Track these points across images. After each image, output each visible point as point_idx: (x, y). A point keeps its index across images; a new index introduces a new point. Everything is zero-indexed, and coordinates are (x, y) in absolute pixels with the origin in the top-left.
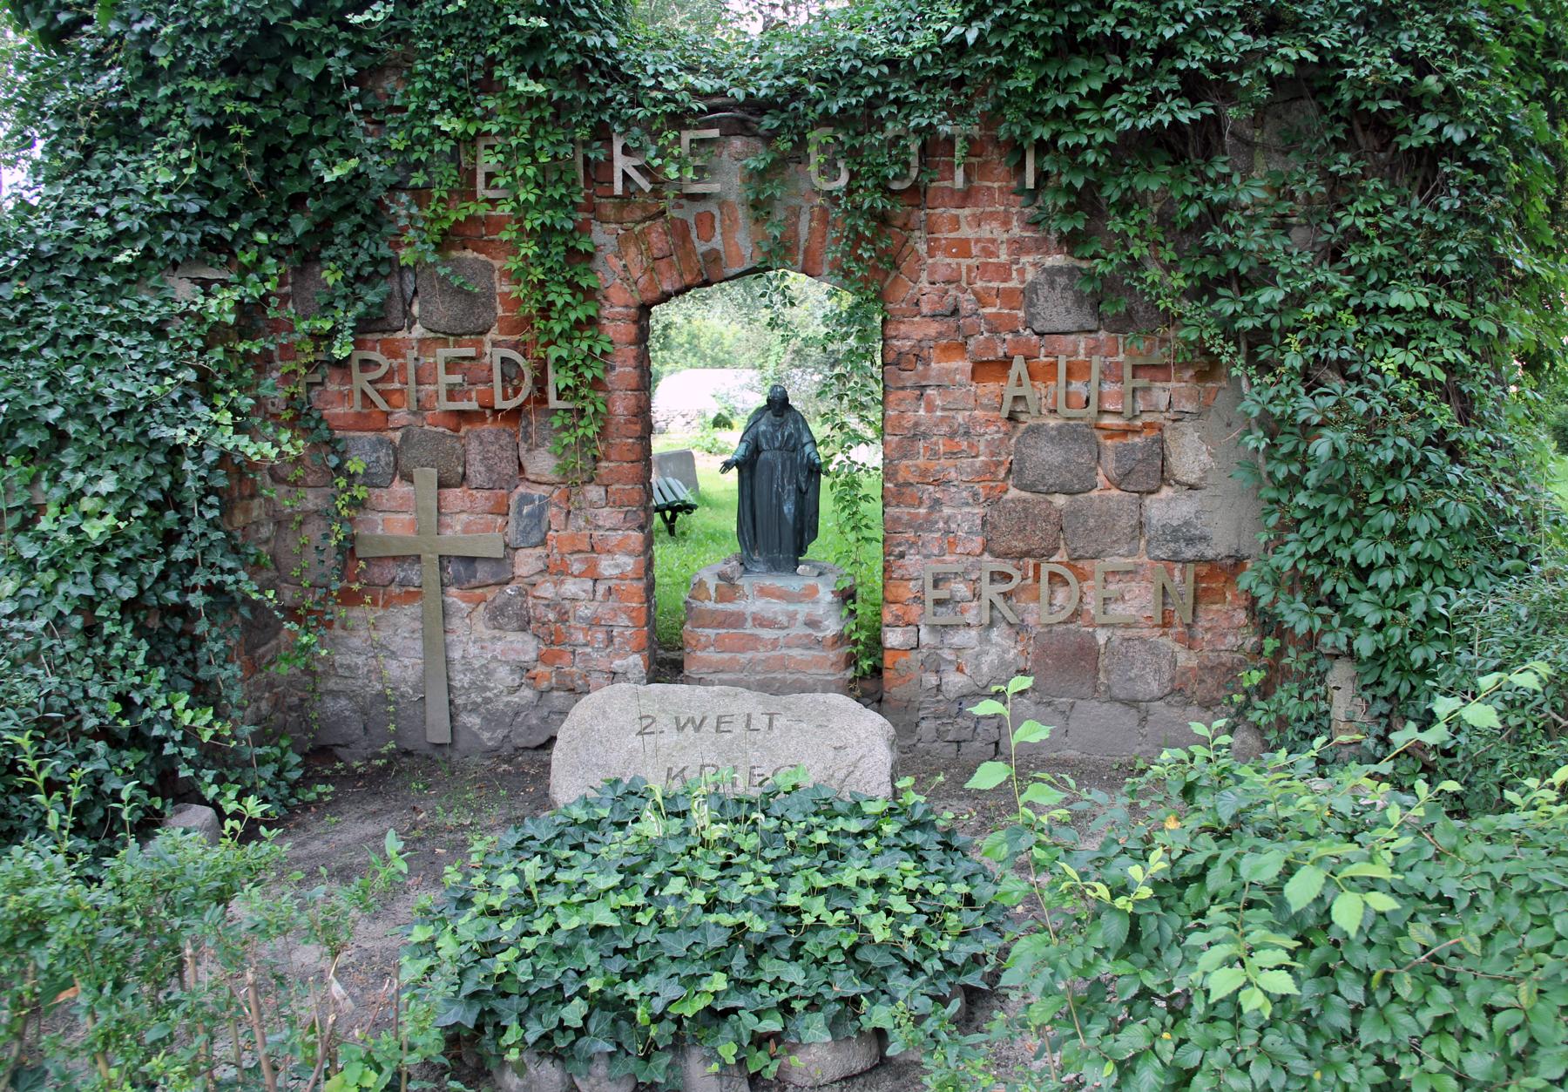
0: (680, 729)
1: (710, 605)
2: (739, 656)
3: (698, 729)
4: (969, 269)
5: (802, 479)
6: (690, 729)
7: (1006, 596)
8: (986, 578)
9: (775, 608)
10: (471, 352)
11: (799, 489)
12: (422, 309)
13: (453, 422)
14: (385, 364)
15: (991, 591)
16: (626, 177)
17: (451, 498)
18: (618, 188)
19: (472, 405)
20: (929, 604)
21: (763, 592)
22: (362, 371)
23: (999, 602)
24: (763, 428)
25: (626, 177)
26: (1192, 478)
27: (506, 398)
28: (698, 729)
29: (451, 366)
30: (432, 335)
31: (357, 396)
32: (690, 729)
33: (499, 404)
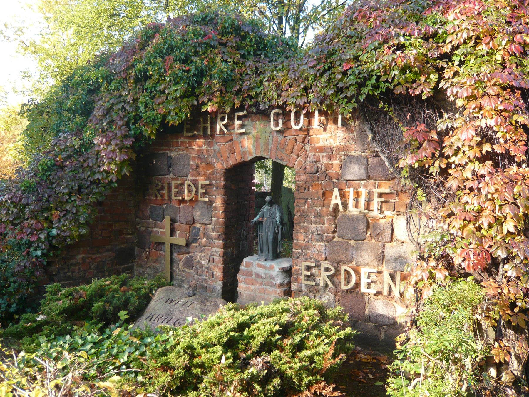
4: (323, 157)
9: (261, 271)
21: (260, 266)
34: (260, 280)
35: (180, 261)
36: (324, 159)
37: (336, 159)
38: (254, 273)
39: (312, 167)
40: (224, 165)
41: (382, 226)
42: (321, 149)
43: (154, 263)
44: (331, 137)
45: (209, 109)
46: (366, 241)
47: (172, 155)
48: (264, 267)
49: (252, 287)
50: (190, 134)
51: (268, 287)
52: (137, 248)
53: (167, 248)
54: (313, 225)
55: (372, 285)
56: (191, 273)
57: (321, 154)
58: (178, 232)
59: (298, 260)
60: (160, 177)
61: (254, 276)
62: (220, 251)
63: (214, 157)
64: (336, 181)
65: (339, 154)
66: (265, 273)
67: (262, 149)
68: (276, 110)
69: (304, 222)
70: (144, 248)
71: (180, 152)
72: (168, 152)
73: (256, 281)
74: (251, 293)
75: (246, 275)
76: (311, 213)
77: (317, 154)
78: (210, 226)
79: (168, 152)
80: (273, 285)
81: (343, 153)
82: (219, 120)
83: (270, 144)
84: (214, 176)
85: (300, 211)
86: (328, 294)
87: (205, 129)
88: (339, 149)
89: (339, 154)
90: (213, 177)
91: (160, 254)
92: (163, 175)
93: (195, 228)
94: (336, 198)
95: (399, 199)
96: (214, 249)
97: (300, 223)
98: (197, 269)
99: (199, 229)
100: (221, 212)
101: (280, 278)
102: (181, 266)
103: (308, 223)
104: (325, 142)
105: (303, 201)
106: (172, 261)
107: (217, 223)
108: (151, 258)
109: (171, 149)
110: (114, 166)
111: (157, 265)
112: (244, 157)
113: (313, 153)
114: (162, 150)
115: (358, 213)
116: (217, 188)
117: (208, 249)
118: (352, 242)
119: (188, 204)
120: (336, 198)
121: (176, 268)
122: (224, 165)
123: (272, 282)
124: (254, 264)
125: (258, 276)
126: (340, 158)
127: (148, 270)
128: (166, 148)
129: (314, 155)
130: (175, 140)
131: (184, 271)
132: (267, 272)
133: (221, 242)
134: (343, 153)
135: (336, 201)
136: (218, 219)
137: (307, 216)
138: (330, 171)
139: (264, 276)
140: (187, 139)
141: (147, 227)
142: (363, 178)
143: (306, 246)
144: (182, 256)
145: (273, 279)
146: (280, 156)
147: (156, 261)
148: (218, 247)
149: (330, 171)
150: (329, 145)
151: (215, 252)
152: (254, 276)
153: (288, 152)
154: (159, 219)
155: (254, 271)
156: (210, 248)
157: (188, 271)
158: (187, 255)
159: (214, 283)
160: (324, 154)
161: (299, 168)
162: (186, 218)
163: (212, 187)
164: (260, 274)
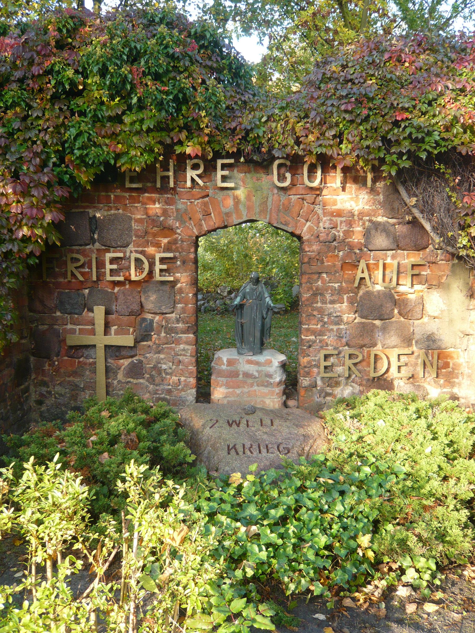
0: (230, 425)
1: (224, 367)
2: (236, 390)
3: (238, 425)
4: (341, 222)
5: (264, 313)
6: (234, 426)
7: (355, 364)
8: (347, 357)
9: (251, 369)
10: (121, 255)
11: (263, 317)
12: (99, 235)
13: (112, 285)
14: (82, 260)
15: (349, 363)
16: (193, 180)
17: (149, 308)
18: (189, 184)
19: (121, 279)
20: (322, 368)
21: (250, 362)
22: (72, 262)
23: (353, 368)
24: (248, 290)
25: (193, 180)
26: (436, 314)
27: (136, 276)
28: (238, 425)
29: (112, 261)
30: (103, 247)
31: (69, 274)
32: (234, 426)
33: (133, 278)
34: (250, 381)
35: (119, 369)
36: (344, 224)
37: (358, 225)
38: (241, 373)
39: (328, 235)
40: (195, 230)
41: (413, 302)
42: (339, 214)
43: (69, 377)
44: (352, 199)
45: (188, 151)
46: (393, 319)
47: (98, 215)
48: (257, 363)
49: (238, 391)
50: (134, 186)
51: (261, 388)
52: (32, 359)
53: (100, 353)
54: (329, 305)
55: (403, 369)
56: (141, 384)
57: (339, 219)
58: (116, 327)
59: (311, 349)
60: (74, 247)
61: (241, 376)
62: (191, 348)
63: (177, 219)
64: (358, 251)
65: (362, 219)
66: (257, 371)
67: (258, 210)
68: (281, 161)
69: (317, 302)
70: (48, 357)
71: (113, 212)
72: (90, 211)
73: (245, 382)
74: (236, 399)
75: (229, 377)
76: (327, 290)
77: (334, 219)
78: (173, 315)
79: (90, 211)
80: (269, 384)
81: (368, 218)
82: (188, 168)
83: (269, 204)
84: (178, 245)
85: (312, 289)
86: (351, 386)
87: (165, 179)
88: (362, 214)
89: (362, 219)
90: (177, 248)
91: (79, 362)
92: (81, 245)
93: (144, 320)
94: (363, 272)
95: (431, 271)
96: (182, 346)
97: (312, 303)
98: (152, 377)
99: (152, 321)
100: (191, 295)
101: (278, 374)
102: (120, 376)
103: (323, 304)
104: (344, 205)
105: (316, 276)
106: (108, 370)
107: (184, 310)
108: (62, 370)
109: (94, 207)
110: (40, 230)
111: (76, 380)
112: (227, 220)
113: (328, 218)
114: (77, 207)
115: (383, 289)
116: (184, 262)
117: (171, 348)
118: (377, 322)
119: (127, 286)
120: (363, 272)
121: (114, 379)
122: (195, 230)
123: (268, 381)
124: (241, 360)
125: (247, 375)
126: (364, 224)
127: (58, 389)
128: (87, 204)
129: (331, 220)
130: (103, 194)
131: (129, 382)
132: (260, 369)
133: (191, 336)
134: (368, 218)
135: (362, 276)
136: (186, 304)
137: (321, 294)
138: (350, 240)
139: (256, 374)
140: (126, 192)
141: (51, 326)
142: (391, 247)
143: (321, 331)
144: (122, 361)
145: (270, 376)
146: (283, 220)
147: (75, 374)
148: (187, 343)
149: (350, 240)
150: (350, 208)
151: (184, 350)
152: (241, 376)
153: (295, 215)
154: (77, 311)
155: (241, 369)
156: (173, 345)
157: (135, 381)
158: (130, 360)
159: (183, 393)
160: (344, 219)
161: (309, 235)
162: (128, 307)
163: (174, 261)
164: (251, 372)
